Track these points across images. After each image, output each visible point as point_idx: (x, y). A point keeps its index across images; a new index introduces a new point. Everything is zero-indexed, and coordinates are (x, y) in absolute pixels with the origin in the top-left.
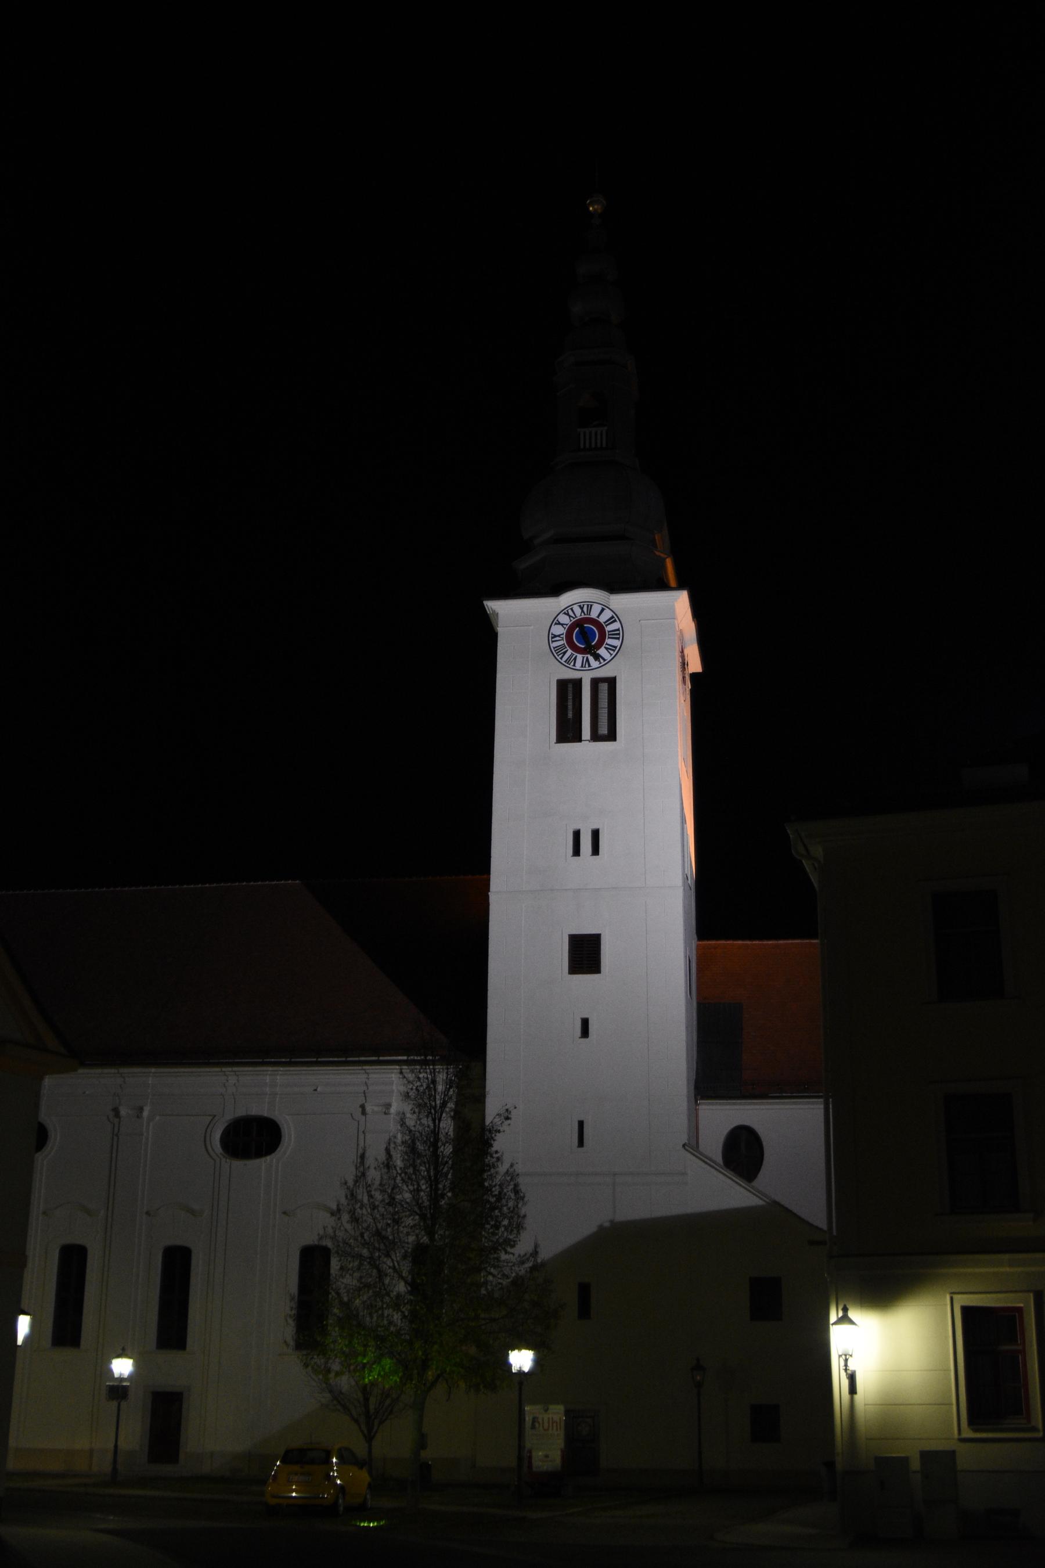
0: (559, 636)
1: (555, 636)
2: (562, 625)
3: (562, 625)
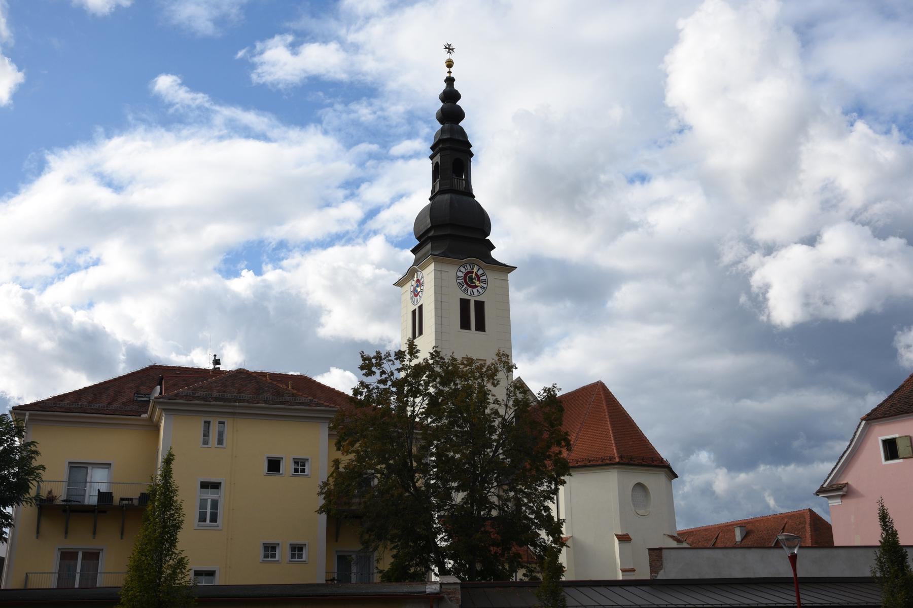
1: (459, 277)
2: (462, 272)
3: (462, 272)
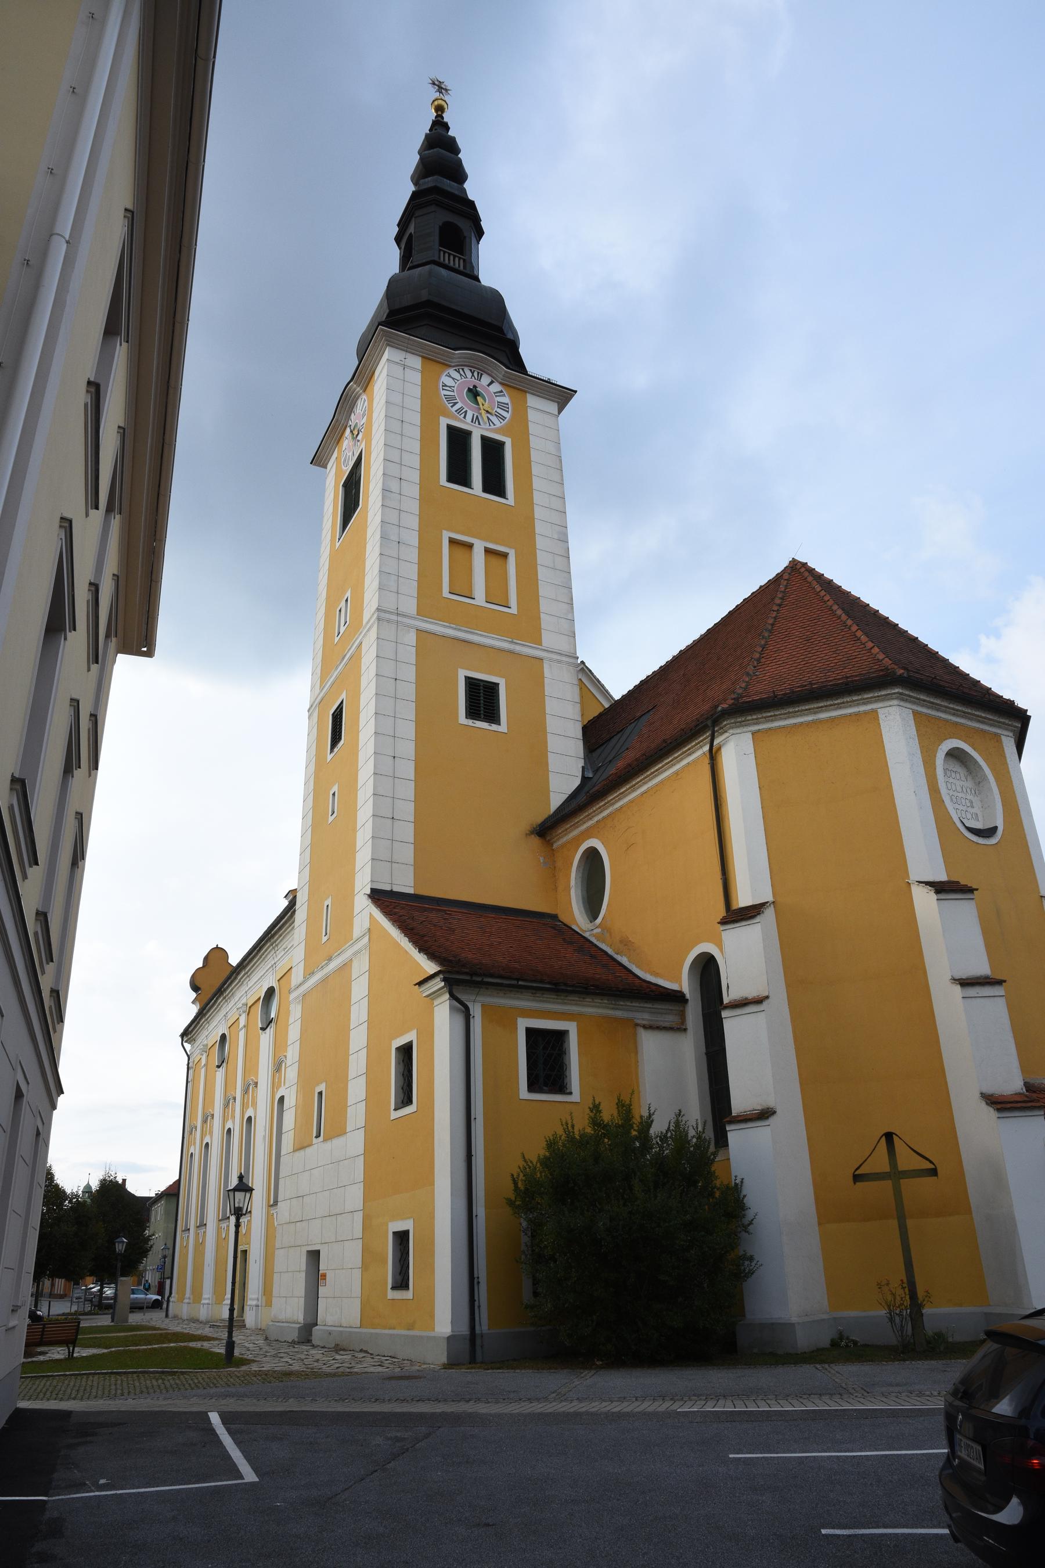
0: (450, 387)
1: (446, 386)
2: (453, 379)
3: (453, 379)
